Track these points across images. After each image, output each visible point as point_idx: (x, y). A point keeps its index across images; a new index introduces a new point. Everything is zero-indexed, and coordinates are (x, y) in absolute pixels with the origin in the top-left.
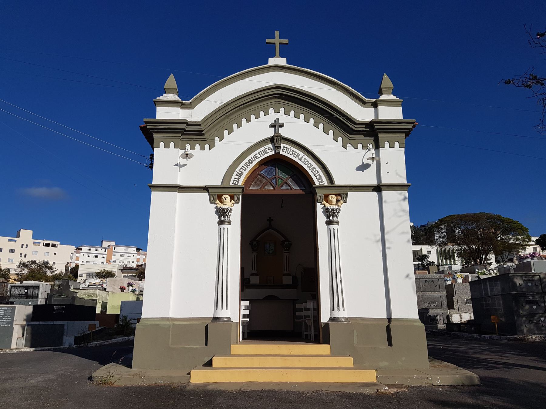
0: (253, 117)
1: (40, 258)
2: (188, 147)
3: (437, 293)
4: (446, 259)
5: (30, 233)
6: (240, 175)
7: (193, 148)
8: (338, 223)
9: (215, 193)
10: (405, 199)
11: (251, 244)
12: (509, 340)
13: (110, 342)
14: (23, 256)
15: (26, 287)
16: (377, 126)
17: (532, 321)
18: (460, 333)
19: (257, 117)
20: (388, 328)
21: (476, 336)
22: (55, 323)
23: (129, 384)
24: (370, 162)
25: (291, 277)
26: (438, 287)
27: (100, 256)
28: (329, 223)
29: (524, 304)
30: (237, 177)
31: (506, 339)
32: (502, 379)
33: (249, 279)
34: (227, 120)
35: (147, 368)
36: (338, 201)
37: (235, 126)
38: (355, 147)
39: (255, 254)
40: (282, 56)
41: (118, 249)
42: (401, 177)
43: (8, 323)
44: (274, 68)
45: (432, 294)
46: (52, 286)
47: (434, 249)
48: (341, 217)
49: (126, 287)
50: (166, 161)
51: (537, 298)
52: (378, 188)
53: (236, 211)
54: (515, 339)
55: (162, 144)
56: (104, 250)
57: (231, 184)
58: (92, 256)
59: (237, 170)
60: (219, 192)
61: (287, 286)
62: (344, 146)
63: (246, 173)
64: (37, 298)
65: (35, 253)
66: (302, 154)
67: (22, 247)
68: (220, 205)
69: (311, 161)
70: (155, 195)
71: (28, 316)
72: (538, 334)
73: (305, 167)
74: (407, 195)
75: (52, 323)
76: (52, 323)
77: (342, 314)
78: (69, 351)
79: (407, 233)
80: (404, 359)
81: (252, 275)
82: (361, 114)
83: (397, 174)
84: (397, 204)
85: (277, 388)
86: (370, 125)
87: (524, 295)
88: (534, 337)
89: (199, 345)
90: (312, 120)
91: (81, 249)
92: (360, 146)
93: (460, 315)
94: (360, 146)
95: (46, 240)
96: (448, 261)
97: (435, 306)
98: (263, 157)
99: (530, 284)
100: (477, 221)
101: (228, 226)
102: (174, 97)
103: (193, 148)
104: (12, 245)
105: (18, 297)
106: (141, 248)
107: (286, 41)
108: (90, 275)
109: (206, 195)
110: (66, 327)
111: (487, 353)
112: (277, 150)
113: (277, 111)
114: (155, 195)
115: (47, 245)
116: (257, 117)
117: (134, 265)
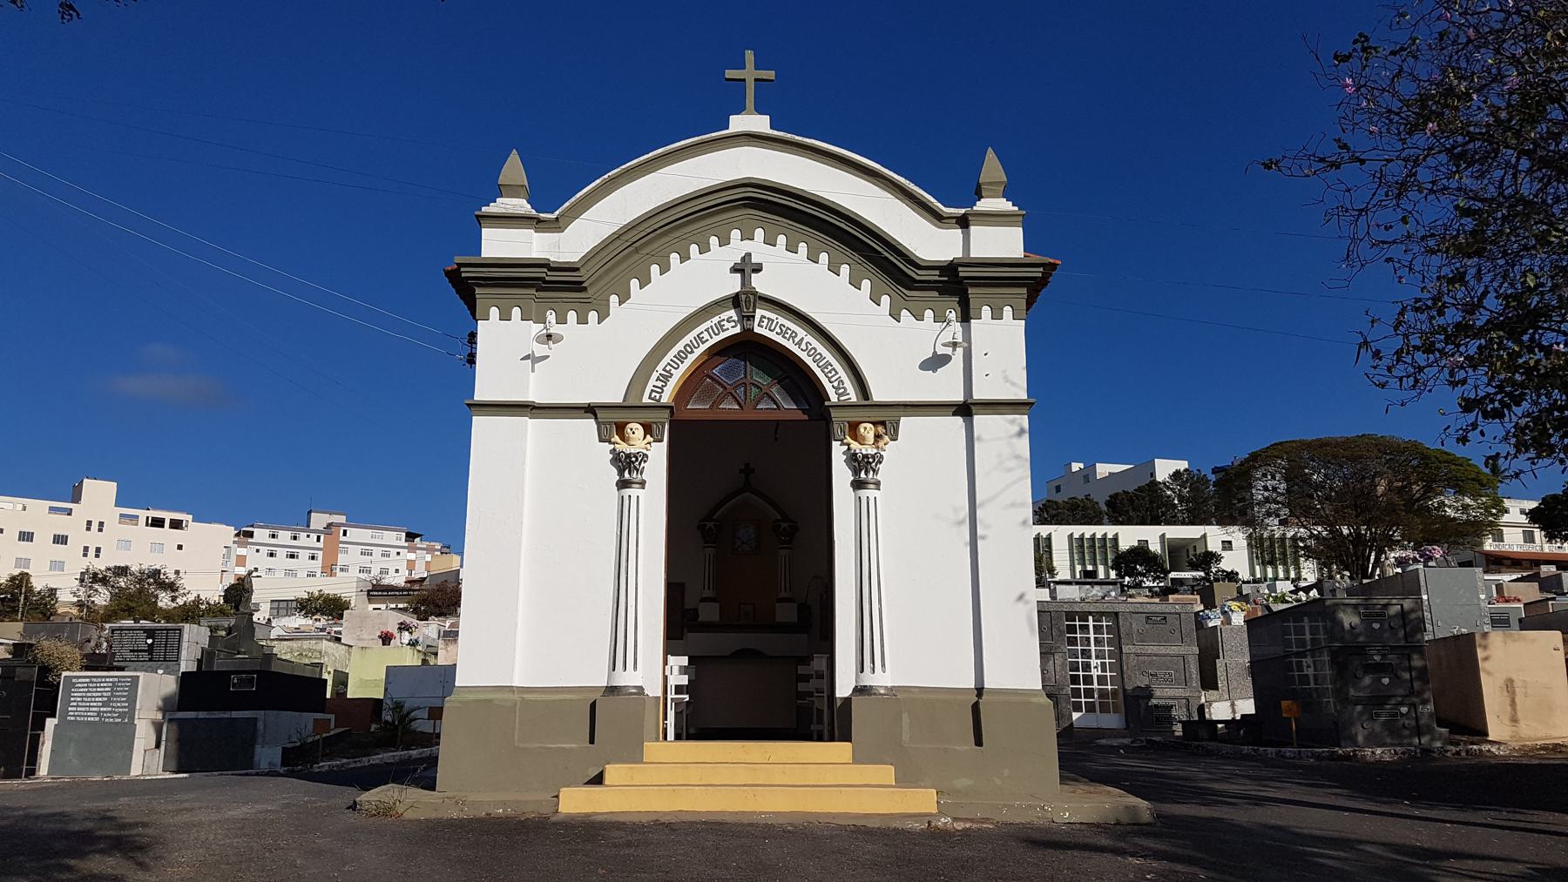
0: (694, 248)
1: (139, 560)
2: (551, 317)
3: (1174, 650)
4: (1264, 564)
5: (112, 487)
6: (665, 378)
7: (562, 320)
8: (877, 485)
9: (610, 419)
10: (1022, 431)
11: (701, 528)
12: (1318, 757)
13: (365, 761)
14: (92, 552)
15: (150, 633)
16: (963, 272)
17: (1378, 715)
18: (1213, 745)
19: (704, 249)
20: (976, 708)
21: (1246, 749)
22: (235, 714)
23: (433, 815)
24: (949, 351)
25: (795, 606)
26: (1177, 633)
27: (304, 555)
28: (858, 485)
29: (1360, 673)
30: (660, 384)
31: (1313, 755)
32: (1214, 819)
33: (696, 611)
34: (637, 257)
35: (468, 784)
36: (878, 437)
37: (655, 269)
38: (919, 317)
39: (709, 551)
40: (760, 110)
41: (355, 534)
42: (1014, 384)
43: (121, 715)
44: (742, 139)
45: (1162, 650)
46: (213, 630)
47: (1238, 536)
48: (884, 472)
49: (396, 632)
50: (505, 347)
51: (1392, 658)
52: (965, 410)
53: (658, 455)
54: (1333, 757)
55: (494, 312)
56: (314, 536)
57: (646, 400)
58: (281, 553)
59: (660, 368)
60: (619, 416)
61: (785, 628)
62: (895, 315)
63: (678, 375)
64: (178, 659)
65: (125, 544)
66: (801, 333)
67: (88, 529)
68: (622, 447)
69: (821, 349)
70: (481, 426)
71: (166, 700)
72: (1392, 745)
73: (809, 361)
74: (1026, 425)
75: (227, 715)
76: (227, 715)
77: (880, 679)
78: (272, 774)
79: (1023, 505)
80: (1006, 772)
81: (703, 600)
82: (931, 243)
83: (1006, 379)
84: (1005, 444)
85: (729, 819)
86: (950, 268)
87: (1360, 650)
88: (1379, 751)
89: (579, 742)
90: (824, 257)
91: (251, 535)
92: (929, 314)
93: (1233, 705)
94: (929, 314)
95: (155, 508)
96: (1270, 570)
97: (1169, 681)
98: (716, 339)
99: (1376, 626)
100: (1354, 459)
101: (639, 492)
102: (520, 205)
103: (562, 320)
104: (61, 524)
105: (129, 656)
106: (454, 543)
107: (771, 75)
108: (281, 607)
109: (590, 424)
110: (260, 725)
111: (1241, 780)
112: (747, 325)
113: (748, 236)
114: (481, 426)
115: (158, 523)
116: (704, 249)
117: (399, 580)
